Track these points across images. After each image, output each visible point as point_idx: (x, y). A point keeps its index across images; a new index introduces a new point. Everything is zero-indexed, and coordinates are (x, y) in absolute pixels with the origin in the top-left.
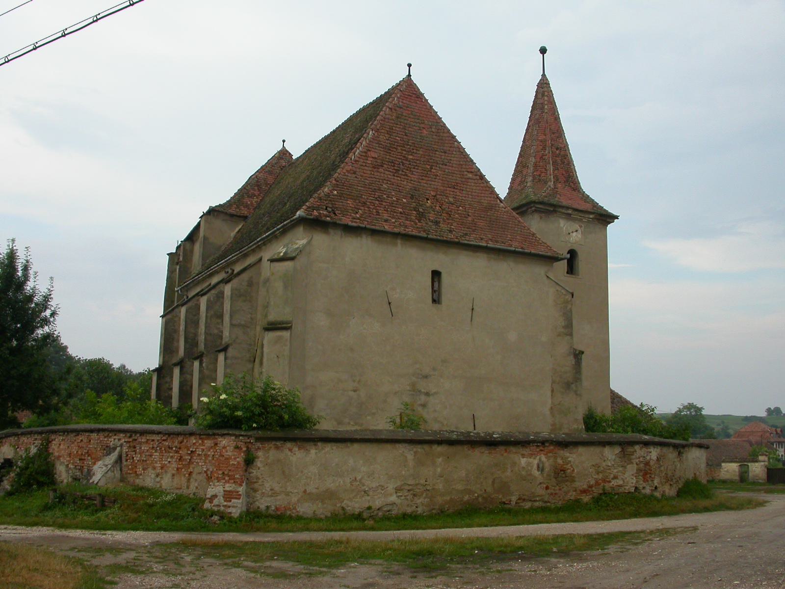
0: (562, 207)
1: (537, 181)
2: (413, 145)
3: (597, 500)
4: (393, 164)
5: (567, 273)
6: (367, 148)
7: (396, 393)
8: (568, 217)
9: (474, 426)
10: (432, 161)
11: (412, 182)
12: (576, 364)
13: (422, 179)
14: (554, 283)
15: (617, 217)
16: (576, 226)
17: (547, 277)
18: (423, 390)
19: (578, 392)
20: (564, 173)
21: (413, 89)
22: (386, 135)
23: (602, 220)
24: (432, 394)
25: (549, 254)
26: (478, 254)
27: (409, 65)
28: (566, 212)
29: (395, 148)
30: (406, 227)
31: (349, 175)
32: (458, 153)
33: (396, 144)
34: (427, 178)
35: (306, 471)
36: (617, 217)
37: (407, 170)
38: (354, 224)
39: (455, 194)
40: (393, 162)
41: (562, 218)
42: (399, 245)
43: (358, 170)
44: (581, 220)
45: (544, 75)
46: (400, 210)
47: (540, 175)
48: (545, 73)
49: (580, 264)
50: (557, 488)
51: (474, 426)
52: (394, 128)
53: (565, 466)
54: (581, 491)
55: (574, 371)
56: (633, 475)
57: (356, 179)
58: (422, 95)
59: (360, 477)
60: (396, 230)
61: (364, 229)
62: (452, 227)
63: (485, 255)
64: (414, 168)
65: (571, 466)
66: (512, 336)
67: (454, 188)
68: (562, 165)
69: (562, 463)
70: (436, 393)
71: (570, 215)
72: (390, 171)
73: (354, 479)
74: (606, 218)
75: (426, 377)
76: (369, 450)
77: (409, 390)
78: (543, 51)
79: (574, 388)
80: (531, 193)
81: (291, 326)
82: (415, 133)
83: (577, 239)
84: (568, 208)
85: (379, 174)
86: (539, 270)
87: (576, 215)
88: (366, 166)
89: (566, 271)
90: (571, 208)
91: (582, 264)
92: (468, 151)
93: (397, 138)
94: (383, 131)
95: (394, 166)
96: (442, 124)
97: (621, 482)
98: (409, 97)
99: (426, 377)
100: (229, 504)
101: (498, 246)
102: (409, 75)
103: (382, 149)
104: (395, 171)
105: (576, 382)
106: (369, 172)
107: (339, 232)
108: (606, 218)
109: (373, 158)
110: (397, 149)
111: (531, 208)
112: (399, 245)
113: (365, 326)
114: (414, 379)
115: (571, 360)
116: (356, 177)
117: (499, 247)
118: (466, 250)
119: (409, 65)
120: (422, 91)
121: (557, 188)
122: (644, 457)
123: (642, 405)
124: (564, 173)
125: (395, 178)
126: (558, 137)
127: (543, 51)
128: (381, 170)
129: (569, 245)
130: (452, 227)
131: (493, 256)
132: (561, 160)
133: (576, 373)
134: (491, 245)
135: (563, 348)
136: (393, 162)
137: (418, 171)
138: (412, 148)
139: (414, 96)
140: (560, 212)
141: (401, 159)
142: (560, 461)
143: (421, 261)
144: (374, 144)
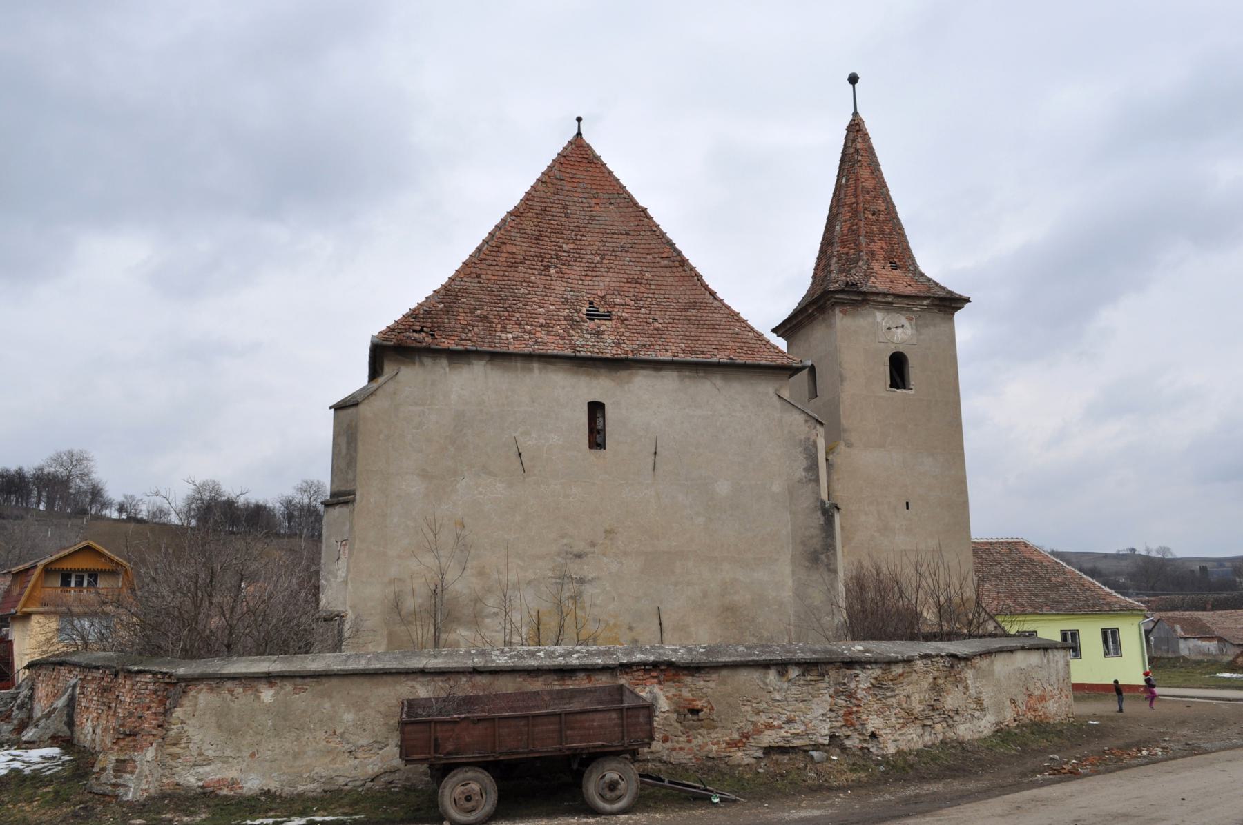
0: (877, 294)
5: (891, 386)
7: (529, 583)
8: (888, 307)
15: (967, 300)
16: (903, 320)
26: (663, 373)
27: (579, 119)
31: (469, 280)
35: (255, 724)
36: (967, 300)
38: (460, 348)
41: (879, 309)
42: (536, 371)
44: (909, 310)
45: (855, 113)
50: (683, 739)
54: (728, 743)
56: (823, 715)
58: (598, 158)
61: (479, 354)
63: (675, 374)
66: (723, 488)
75: (579, 556)
78: (853, 79)
80: (837, 280)
81: (354, 500)
84: (885, 295)
87: (903, 304)
89: (889, 382)
91: (914, 372)
92: (663, 228)
99: (579, 556)
100: (120, 781)
102: (579, 134)
107: (444, 362)
108: (949, 303)
112: (536, 371)
115: (818, 518)
118: (642, 368)
120: (598, 153)
123: (1148, 550)
127: (853, 79)
128: (521, 268)
129: (892, 346)
143: (571, 392)
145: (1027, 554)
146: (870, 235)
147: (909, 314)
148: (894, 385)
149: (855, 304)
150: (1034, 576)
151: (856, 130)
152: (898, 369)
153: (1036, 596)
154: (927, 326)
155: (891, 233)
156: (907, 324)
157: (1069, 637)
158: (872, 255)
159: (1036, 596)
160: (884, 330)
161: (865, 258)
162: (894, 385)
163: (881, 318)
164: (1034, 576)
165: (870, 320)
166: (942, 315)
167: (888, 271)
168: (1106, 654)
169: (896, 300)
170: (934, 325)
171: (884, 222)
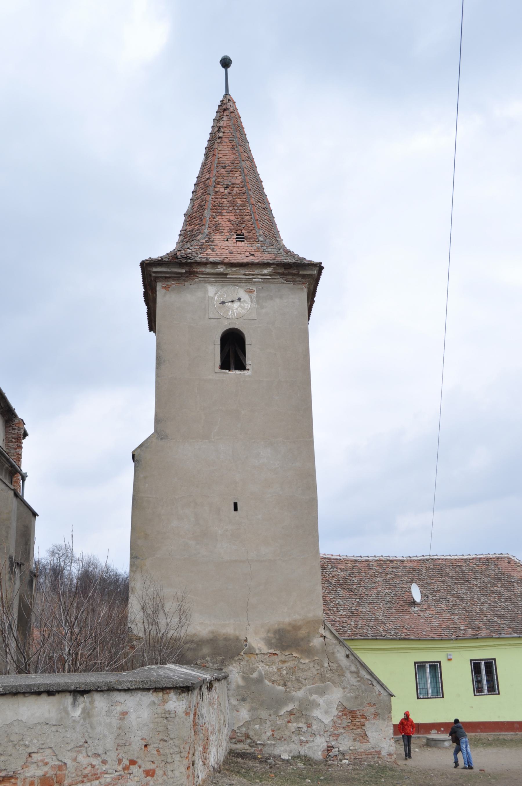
0: (205, 264)
16: (241, 293)
20: (233, 218)
23: (293, 274)
28: (213, 271)
44: (249, 281)
45: (227, 94)
48: (230, 92)
68: (231, 209)
71: (224, 275)
78: (226, 63)
83: (243, 312)
84: (215, 264)
87: (240, 273)
108: (304, 275)
124: (233, 218)
127: (226, 63)
145: (508, 570)
146: (218, 210)
147: (249, 286)
148: (225, 365)
149: (179, 277)
150: (506, 594)
151: (226, 109)
152: (233, 349)
153: (500, 617)
154: (271, 298)
155: (243, 205)
156: (245, 296)
157: (483, 667)
158: (217, 228)
159: (500, 617)
160: (216, 304)
161: (206, 231)
162: (225, 365)
163: (213, 292)
164: (506, 594)
165: (200, 294)
166: (291, 285)
167: (232, 244)
168: (478, 690)
169: (229, 271)
170: (281, 297)
171: (237, 195)
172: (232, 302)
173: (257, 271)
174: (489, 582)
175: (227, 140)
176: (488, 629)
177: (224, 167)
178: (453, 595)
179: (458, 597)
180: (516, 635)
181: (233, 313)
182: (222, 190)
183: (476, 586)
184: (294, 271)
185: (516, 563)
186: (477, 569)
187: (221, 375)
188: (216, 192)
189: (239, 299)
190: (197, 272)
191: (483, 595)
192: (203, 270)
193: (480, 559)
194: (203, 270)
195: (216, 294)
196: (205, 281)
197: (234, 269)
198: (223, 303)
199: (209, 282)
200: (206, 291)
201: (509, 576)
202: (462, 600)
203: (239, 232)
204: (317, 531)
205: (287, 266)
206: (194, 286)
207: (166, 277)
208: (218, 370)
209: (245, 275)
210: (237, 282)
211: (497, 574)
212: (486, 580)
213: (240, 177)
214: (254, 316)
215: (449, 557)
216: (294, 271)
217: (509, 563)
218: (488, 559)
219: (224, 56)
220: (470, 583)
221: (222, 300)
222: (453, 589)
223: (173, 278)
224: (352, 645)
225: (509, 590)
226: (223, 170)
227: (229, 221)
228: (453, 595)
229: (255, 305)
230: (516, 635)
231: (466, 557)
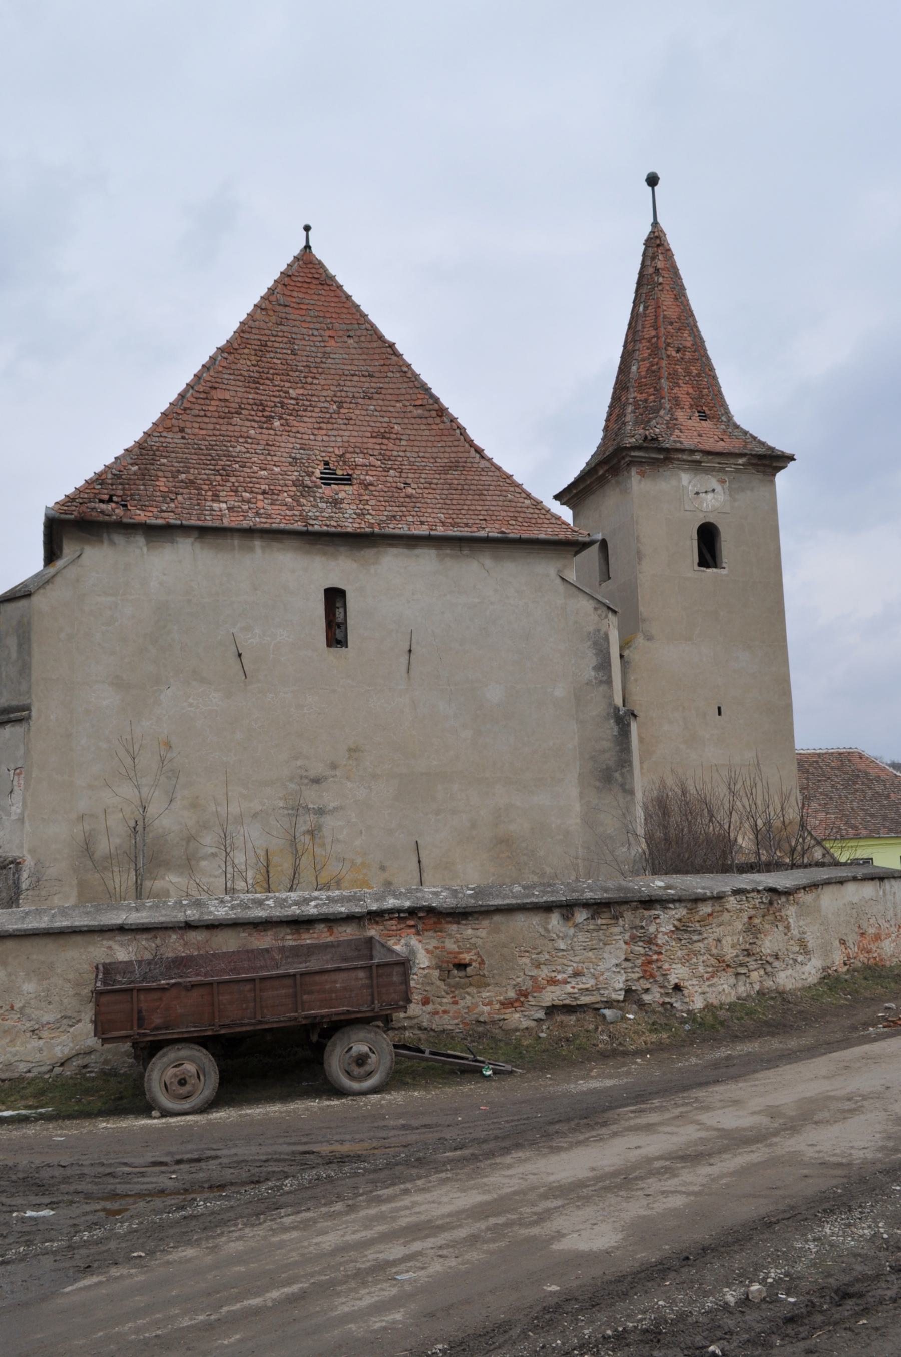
0: (683, 451)
1: (641, 410)
2: (307, 370)
3: (209, 1105)
4: (260, 408)
6: (210, 384)
7: (255, 815)
8: (696, 466)
9: (419, 862)
10: (343, 394)
11: (299, 435)
12: (619, 734)
13: (320, 428)
14: (574, 589)
15: (791, 458)
16: (713, 483)
17: (563, 579)
18: (311, 806)
19: (627, 787)
20: (691, 390)
21: (313, 271)
22: (253, 357)
23: (765, 465)
24: (330, 811)
25: (562, 536)
26: (418, 551)
27: (307, 229)
28: (689, 458)
29: (267, 378)
30: (269, 516)
32: (398, 375)
33: (271, 371)
34: (330, 426)
36: (791, 458)
37: (291, 415)
38: (160, 522)
39: (384, 447)
40: (262, 404)
42: (259, 551)
43: (188, 424)
44: (721, 470)
45: (655, 224)
46: (263, 487)
47: (646, 400)
48: (659, 220)
49: (723, 544)
51: (419, 862)
52: (269, 343)
53: (461, 956)
55: (618, 748)
57: (183, 441)
59: (21, 1005)
60: (246, 524)
62: (367, 507)
64: (305, 410)
65: (478, 954)
67: (384, 437)
68: (687, 378)
69: (457, 950)
70: (336, 809)
71: (700, 462)
72: (254, 421)
73: (8, 1008)
74: (770, 461)
75: (317, 781)
76: (50, 946)
77: (283, 808)
78: (652, 180)
79: (620, 779)
80: (633, 435)
82: (314, 349)
83: (717, 504)
84: (692, 451)
85: (231, 428)
86: (546, 569)
87: (714, 463)
88: (205, 416)
89: (696, 560)
90: (697, 451)
91: (728, 546)
93: (275, 360)
94: (246, 351)
95: (264, 410)
96: (369, 327)
97: (590, 983)
98: (305, 285)
99: (317, 781)
101: (465, 532)
102: (308, 247)
103: (241, 384)
104: (264, 419)
105: (623, 767)
106: (211, 426)
108: (770, 461)
109: (220, 400)
110: (272, 380)
111: (623, 458)
112: (259, 551)
113: (191, 700)
114: (292, 786)
116: (183, 438)
117: (454, 534)
118: (392, 546)
119: (307, 229)
121: (676, 419)
122: (642, 928)
124: (691, 390)
125: (264, 431)
126: (679, 330)
127: (652, 180)
128: (236, 420)
129: (701, 515)
130: (367, 507)
131: (449, 551)
132: (685, 369)
133: (622, 751)
134: (440, 531)
135: (596, 708)
136: (262, 404)
137: (314, 414)
138: (303, 375)
139: (315, 282)
140: (678, 459)
141: (280, 396)
142: (450, 945)
143: (305, 576)
144: (226, 376)
149: (655, 464)
150: (870, 793)
151: (656, 244)
152: (708, 543)
155: (699, 375)
156: (718, 487)
160: (691, 495)
161: (668, 406)
164: (870, 793)
165: (674, 482)
169: (705, 458)
170: (752, 490)
172: (706, 492)
173: (732, 461)
174: (850, 779)
175: (668, 288)
176: (866, 828)
177: (671, 324)
178: (821, 793)
179: (827, 795)
180: (893, 835)
181: (707, 505)
182: (674, 353)
183: (839, 783)
184: (767, 462)
185: (867, 758)
186: (833, 764)
187: (700, 573)
188: (668, 356)
189: (714, 490)
190: (673, 459)
191: (849, 794)
192: (680, 456)
193: (833, 753)
194: (680, 456)
195: (690, 482)
196: (679, 468)
197: (710, 457)
198: (697, 493)
199: (684, 470)
200: (680, 480)
201: (867, 773)
202: (831, 799)
203: (699, 408)
204: (793, 736)
205: (761, 457)
206: (668, 473)
207: (641, 462)
208: (696, 567)
209: (719, 463)
210: (709, 471)
211: (853, 771)
212: (846, 777)
213: (689, 339)
214: (728, 509)
215: (802, 751)
216: (767, 462)
217: (861, 758)
218: (840, 754)
219: (649, 174)
220: (832, 780)
221: (696, 490)
222: (819, 787)
223: (648, 463)
224: (828, 845)
225: (871, 788)
226: (670, 327)
227: (688, 394)
228: (821, 793)
229: (728, 498)
230: (893, 835)
231: (818, 751)
